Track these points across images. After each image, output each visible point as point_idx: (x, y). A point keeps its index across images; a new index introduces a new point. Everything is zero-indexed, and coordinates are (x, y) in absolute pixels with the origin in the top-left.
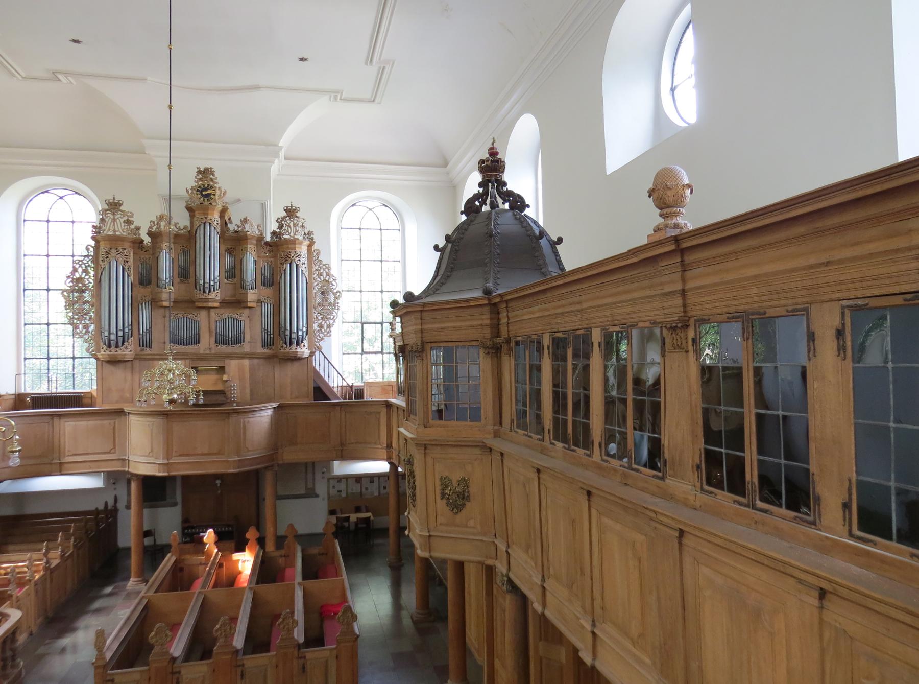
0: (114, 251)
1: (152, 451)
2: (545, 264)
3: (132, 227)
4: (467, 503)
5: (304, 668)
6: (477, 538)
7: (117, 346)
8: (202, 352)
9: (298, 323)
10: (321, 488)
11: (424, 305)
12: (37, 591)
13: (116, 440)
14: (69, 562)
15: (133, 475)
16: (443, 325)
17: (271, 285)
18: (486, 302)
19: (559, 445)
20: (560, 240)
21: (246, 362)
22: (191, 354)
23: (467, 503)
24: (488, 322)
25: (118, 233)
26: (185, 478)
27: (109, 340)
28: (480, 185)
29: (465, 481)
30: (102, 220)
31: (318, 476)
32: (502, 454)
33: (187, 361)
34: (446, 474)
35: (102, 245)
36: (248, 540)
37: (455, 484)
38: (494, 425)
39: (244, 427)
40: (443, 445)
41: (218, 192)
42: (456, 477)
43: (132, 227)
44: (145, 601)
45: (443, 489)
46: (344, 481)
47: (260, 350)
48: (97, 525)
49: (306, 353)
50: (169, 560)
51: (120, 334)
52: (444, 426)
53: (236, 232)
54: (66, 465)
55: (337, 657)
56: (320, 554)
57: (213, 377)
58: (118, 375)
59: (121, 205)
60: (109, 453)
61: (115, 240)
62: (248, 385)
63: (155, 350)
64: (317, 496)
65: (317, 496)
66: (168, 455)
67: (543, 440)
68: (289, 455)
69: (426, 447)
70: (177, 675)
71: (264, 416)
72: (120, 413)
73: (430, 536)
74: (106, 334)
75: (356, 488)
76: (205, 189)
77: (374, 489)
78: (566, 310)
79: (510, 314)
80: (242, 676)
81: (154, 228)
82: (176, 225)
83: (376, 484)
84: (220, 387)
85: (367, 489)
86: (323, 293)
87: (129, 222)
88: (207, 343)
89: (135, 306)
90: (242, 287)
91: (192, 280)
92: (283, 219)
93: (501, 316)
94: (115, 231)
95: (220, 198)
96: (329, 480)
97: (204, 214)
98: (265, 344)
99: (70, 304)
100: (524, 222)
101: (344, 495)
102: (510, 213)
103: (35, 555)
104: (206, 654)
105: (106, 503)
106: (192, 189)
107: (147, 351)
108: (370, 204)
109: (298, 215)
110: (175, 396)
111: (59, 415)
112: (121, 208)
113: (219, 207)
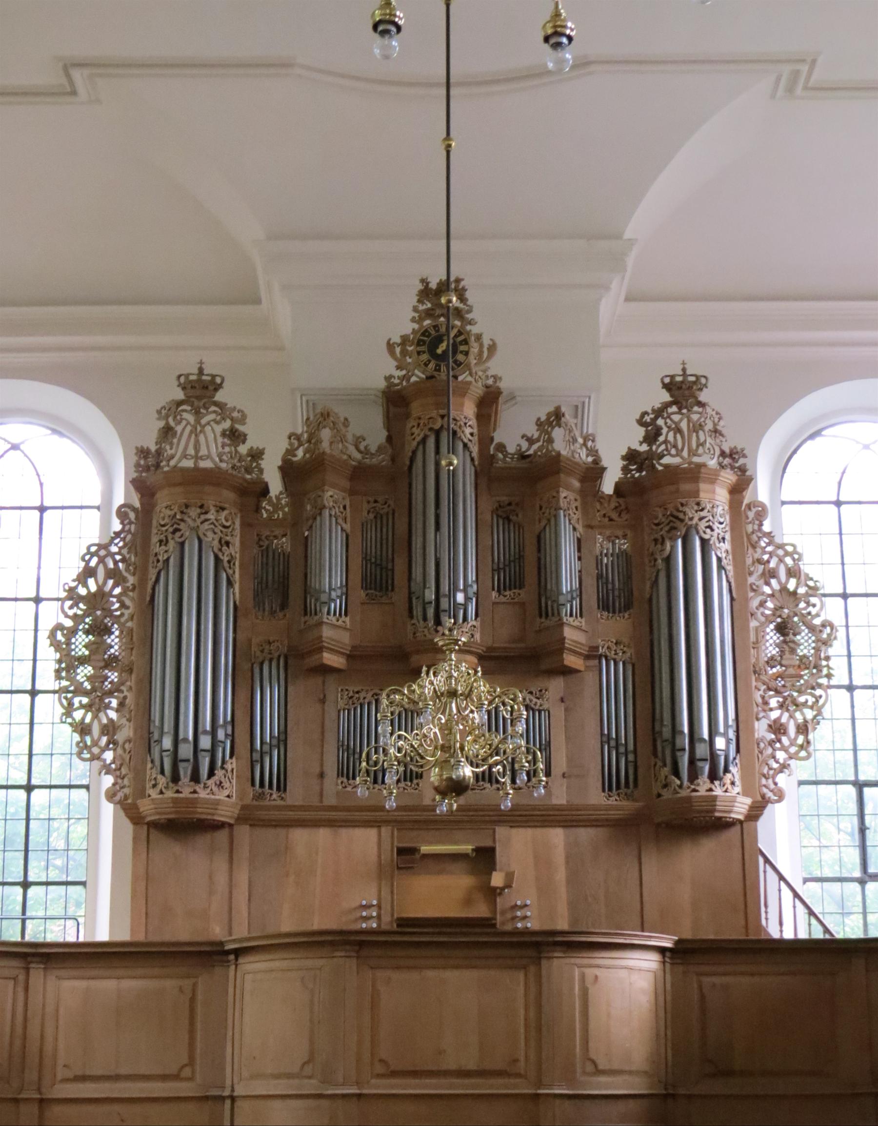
0: (194, 512)
1: (310, 1060)
3: (243, 449)
7: (195, 778)
9: (714, 710)
17: (628, 606)
21: (557, 836)
25: (203, 464)
27: (176, 762)
30: (167, 432)
33: (386, 831)
35: (163, 499)
41: (474, 349)
43: (243, 449)
47: (595, 796)
49: (741, 807)
51: (205, 742)
53: (523, 457)
57: (460, 882)
58: (197, 867)
59: (218, 387)
60: (176, 1077)
61: (198, 480)
74: (167, 743)
76: (441, 337)
81: (300, 453)
82: (358, 441)
84: (481, 910)
86: (782, 629)
87: (235, 436)
89: (244, 673)
90: (543, 612)
91: (399, 597)
92: (659, 412)
94: (197, 458)
97: (438, 406)
98: (610, 784)
106: (405, 340)
109: (703, 397)
112: (219, 397)
113: (477, 390)
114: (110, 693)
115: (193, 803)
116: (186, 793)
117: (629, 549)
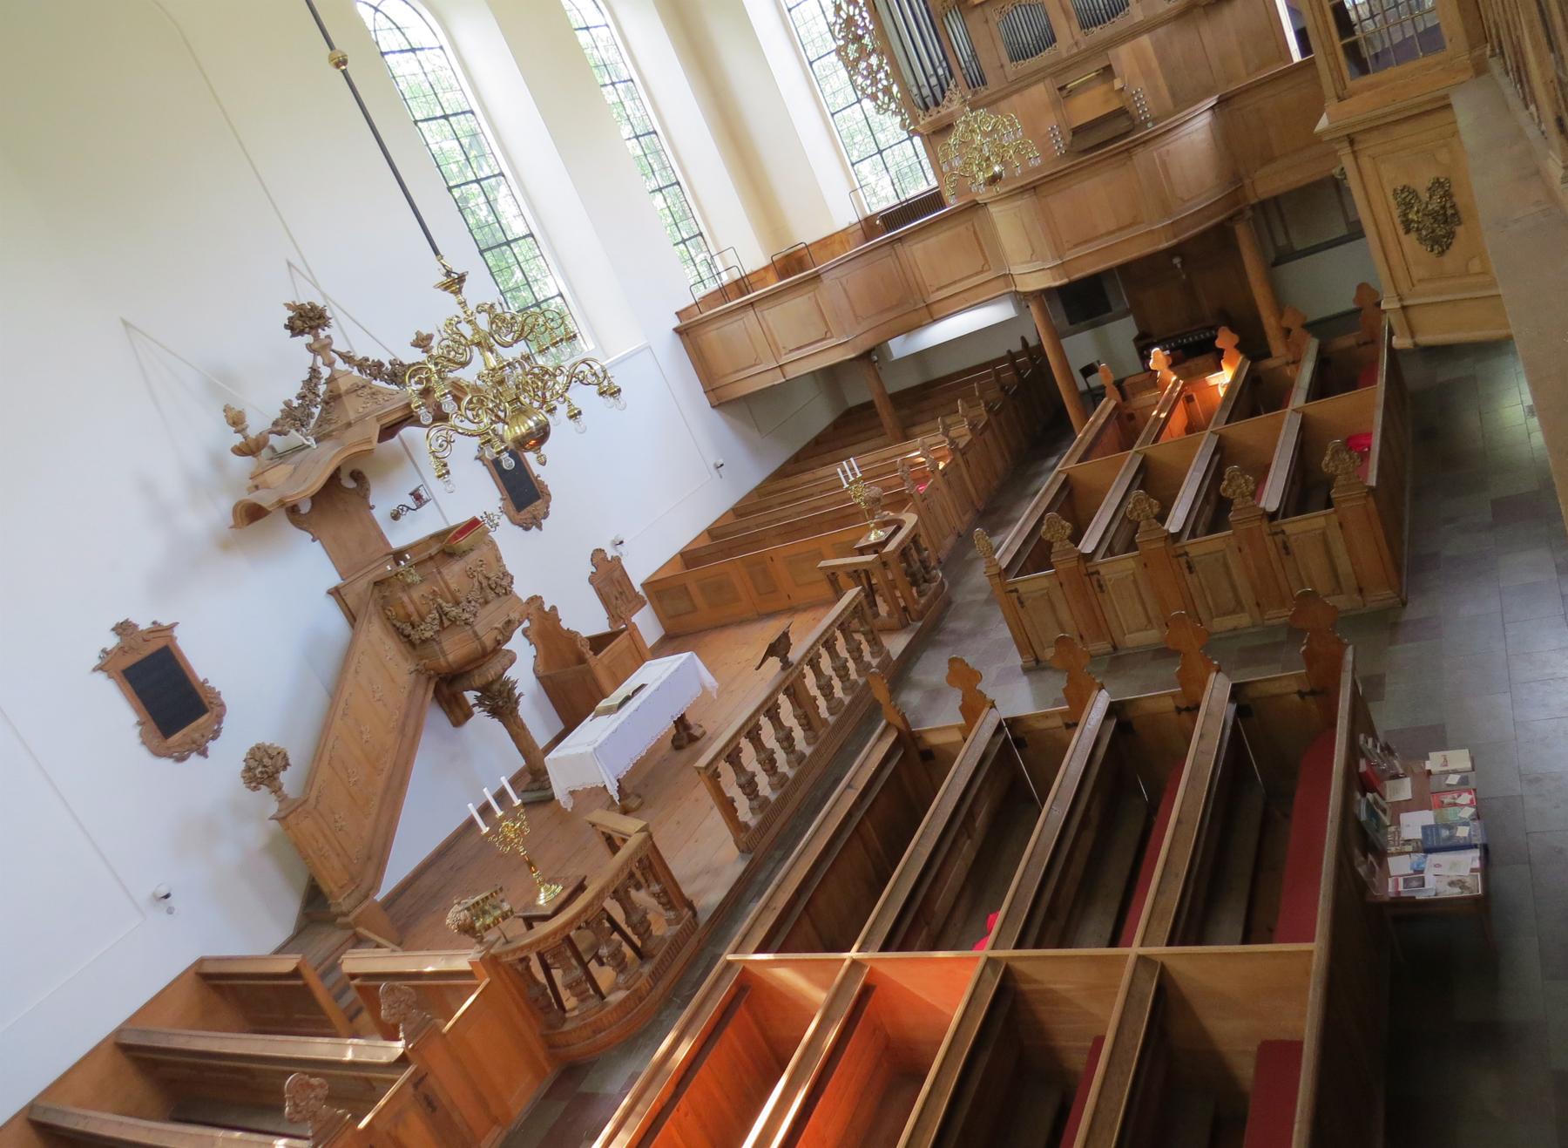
5: (1286, 548)
7: (937, 104)
8: (1065, 55)
12: (949, 483)
13: (985, 248)
14: (987, 434)
21: (1145, 40)
22: (1048, 67)
26: (1124, 268)
27: (923, 99)
29: (1441, 185)
33: (1047, 81)
36: (1222, 351)
37: (1425, 196)
38: (1472, 47)
39: (1164, 163)
42: (1422, 182)
44: (1063, 477)
45: (1405, 215)
48: (1018, 372)
50: (1108, 404)
51: (934, 81)
52: (1370, 87)
54: (935, 307)
55: (1341, 525)
56: (1359, 345)
60: (982, 272)
62: (1161, 83)
63: (993, 84)
66: (1058, 249)
68: (1269, 182)
70: (1095, 577)
71: (1198, 127)
73: (1404, 308)
74: (915, 90)
80: (1190, 569)
84: (1115, 105)
88: (1068, 36)
99: (851, 66)
103: (930, 440)
104: (1131, 546)
105: (1023, 339)
107: (983, 92)
110: (997, 169)
111: (900, 239)
114: (878, 72)
115: (940, 119)
116: (935, 116)
117: (440, 1021)
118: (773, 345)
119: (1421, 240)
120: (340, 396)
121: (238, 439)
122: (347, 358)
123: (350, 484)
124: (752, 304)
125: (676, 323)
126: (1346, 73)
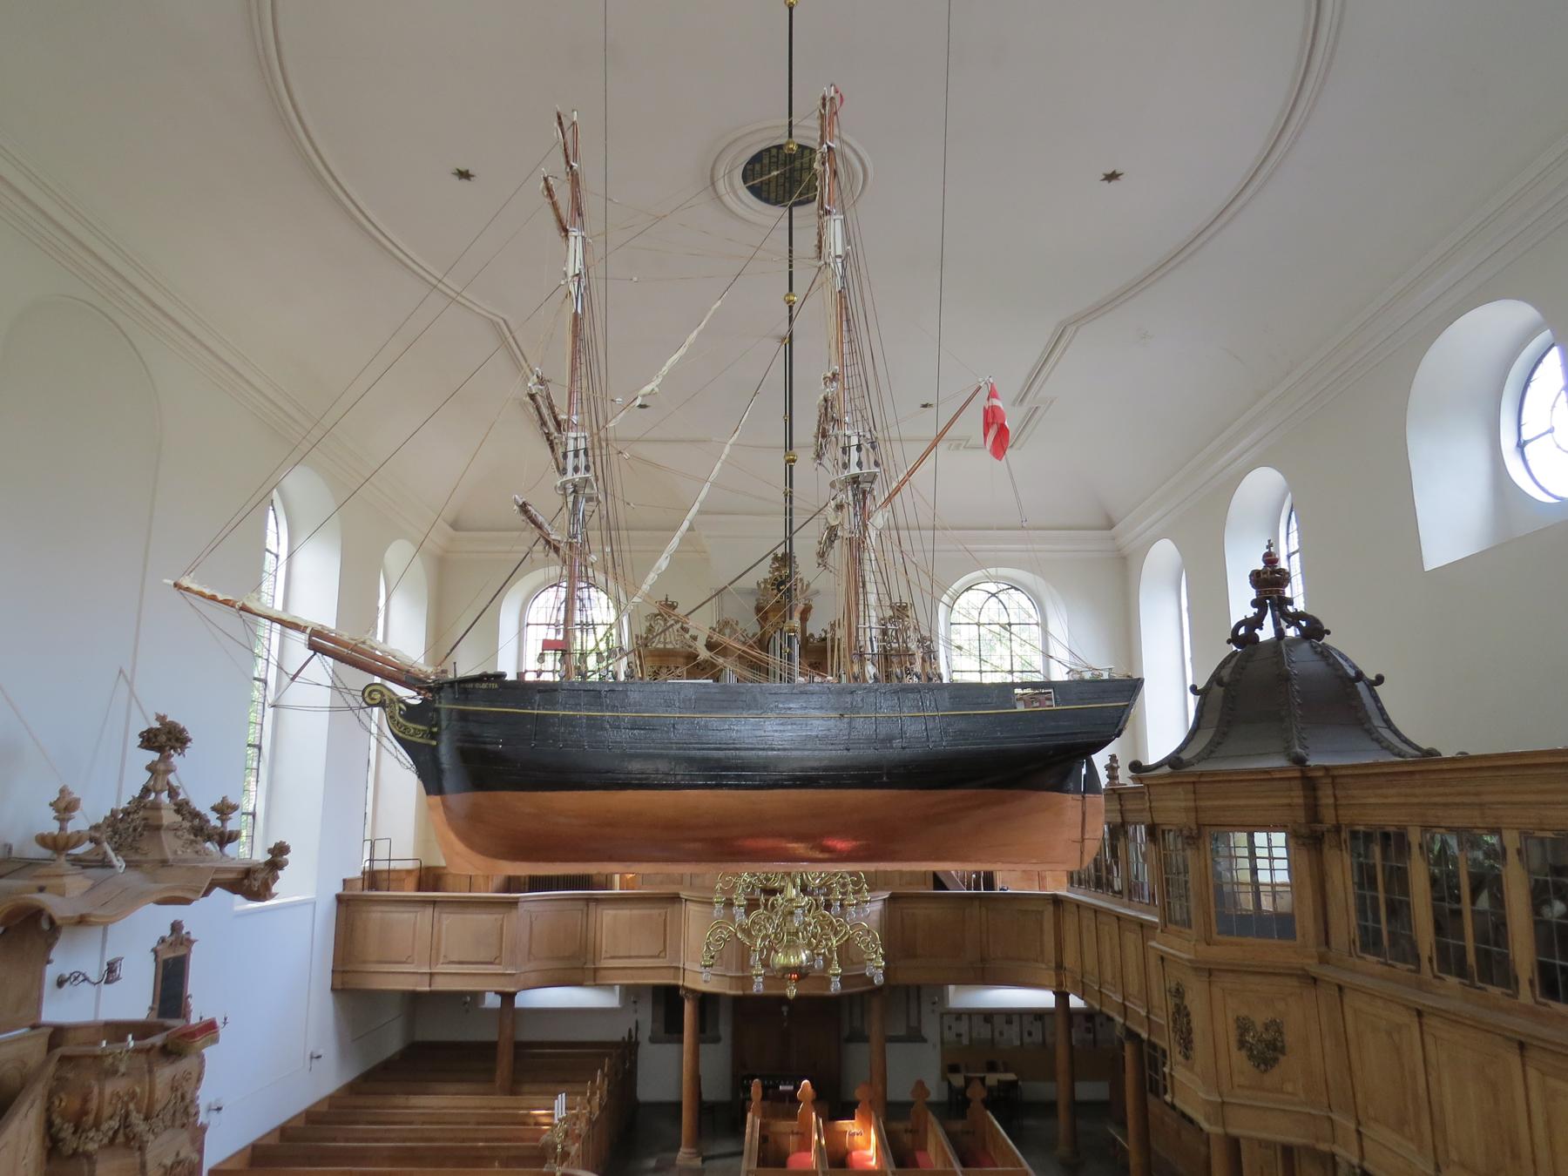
2: (1369, 719)
4: (1282, 1058)
6: (1298, 1109)
10: (931, 1029)
11: (1202, 774)
13: (667, 937)
15: (688, 990)
16: (1226, 802)
18: (1297, 774)
19: (1452, 980)
20: (1380, 680)
23: (1282, 1058)
24: (1301, 801)
25: (669, 646)
28: (1254, 604)
30: (650, 629)
31: (926, 1008)
32: (1340, 988)
34: (1244, 1012)
37: (1260, 1028)
40: (1235, 970)
42: (1260, 1017)
45: (1242, 1035)
46: (965, 1018)
54: (603, 973)
64: (924, 1040)
65: (924, 1040)
67: (1418, 971)
69: (1210, 972)
72: (675, 899)
75: (984, 1032)
77: (1012, 1035)
78: (1450, 800)
79: (1339, 793)
83: (1015, 1028)
85: (1001, 1034)
93: (1320, 793)
95: (803, 592)
96: (942, 1015)
100: (1326, 654)
101: (965, 1041)
102: (1306, 645)
108: (993, 588)
113: (801, 606)
118: (434, 953)
119: (1251, 1057)
120: (158, 828)
121: (53, 827)
122: (173, 793)
123: (45, 926)
124: (434, 903)
125: (339, 890)
126: (1215, 929)
